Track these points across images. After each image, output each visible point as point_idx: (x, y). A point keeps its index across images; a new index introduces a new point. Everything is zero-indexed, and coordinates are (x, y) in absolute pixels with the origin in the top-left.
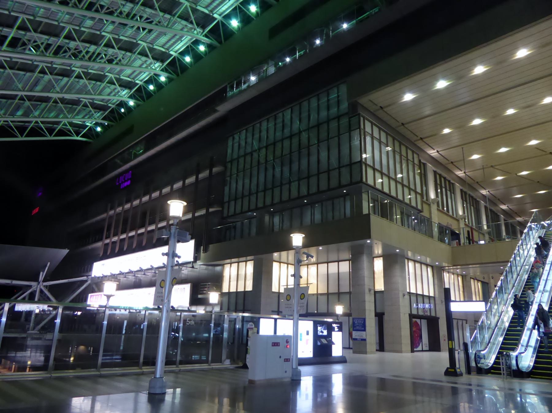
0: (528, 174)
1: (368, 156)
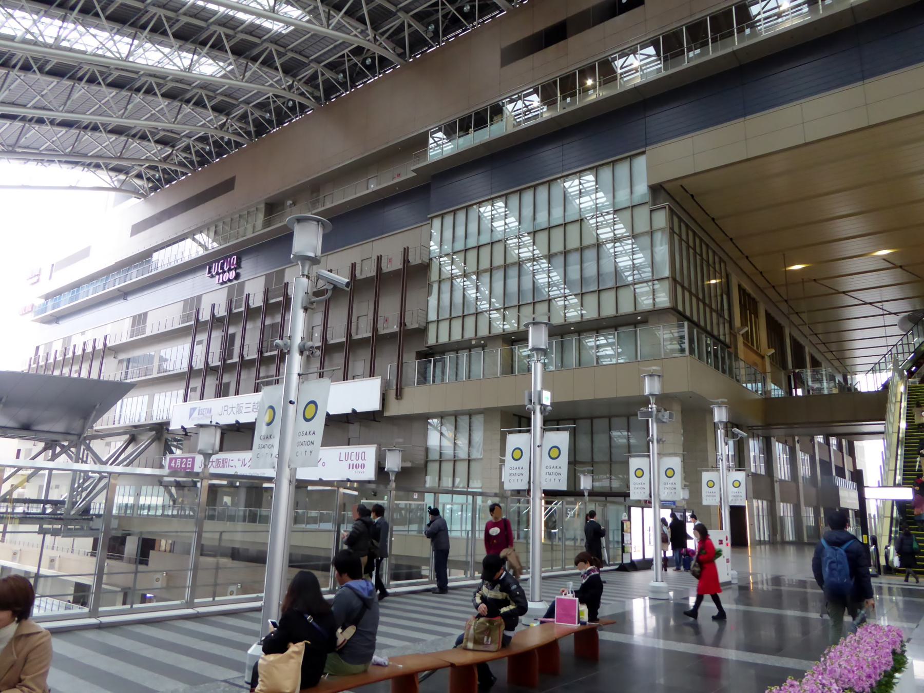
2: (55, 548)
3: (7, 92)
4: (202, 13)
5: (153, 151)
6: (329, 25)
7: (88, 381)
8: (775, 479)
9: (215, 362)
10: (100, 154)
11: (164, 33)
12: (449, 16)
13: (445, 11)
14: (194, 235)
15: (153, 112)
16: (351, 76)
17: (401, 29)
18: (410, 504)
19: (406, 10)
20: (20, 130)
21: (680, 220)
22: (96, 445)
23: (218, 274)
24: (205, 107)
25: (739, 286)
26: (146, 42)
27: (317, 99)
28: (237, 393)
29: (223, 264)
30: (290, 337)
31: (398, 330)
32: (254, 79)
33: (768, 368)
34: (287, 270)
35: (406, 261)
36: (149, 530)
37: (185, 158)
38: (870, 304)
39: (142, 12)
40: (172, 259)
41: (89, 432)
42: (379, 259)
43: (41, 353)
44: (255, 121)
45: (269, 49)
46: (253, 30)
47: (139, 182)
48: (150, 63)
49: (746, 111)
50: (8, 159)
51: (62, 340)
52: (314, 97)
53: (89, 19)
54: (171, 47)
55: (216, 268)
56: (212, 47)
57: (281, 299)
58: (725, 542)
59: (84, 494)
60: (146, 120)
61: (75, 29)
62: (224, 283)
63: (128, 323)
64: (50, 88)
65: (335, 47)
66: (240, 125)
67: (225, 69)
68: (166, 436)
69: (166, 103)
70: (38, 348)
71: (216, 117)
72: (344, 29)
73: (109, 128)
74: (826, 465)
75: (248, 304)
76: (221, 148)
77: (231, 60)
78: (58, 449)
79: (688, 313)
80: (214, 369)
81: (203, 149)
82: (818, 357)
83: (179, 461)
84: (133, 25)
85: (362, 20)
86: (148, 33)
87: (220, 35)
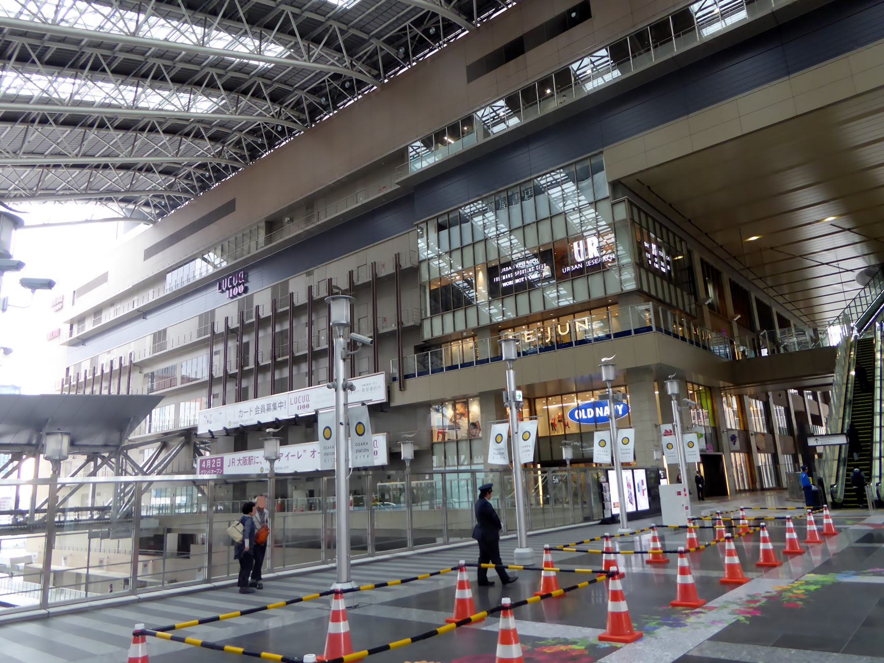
2: (102, 550)
5: (158, 181)
6: (310, 57)
7: (118, 397)
8: (750, 433)
9: (233, 370)
11: (164, 79)
12: (417, 39)
13: (413, 34)
14: (203, 255)
15: (156, 147)
16: (332, 99)
17: (375, 53)
18: (421, 484)
19: (378, 36)
21: (639, 210)
22: (133, 453)
23: (228, 289)
24: (202, 138)
25: (702, 260)
27: (303, 121)
28: (256, 397)
29: (231, 280)
30: (336, 380)
31: (396, 328)
33: (736, 332)
34: (290, 281)
35: (398, 265)
36: (188, 529)
38: (827, 264)
39: (79, 53)
40: (185, 279)
41: (126, 443)
43: (71, 373)
44: (248, 145)
45: (257, 83)
46: (242, 68)
47: (146, 210)
49: (687, 109)
51: (89, 361)
52: (299, 120)
53: (98, 74)
54: (170, 90)
55: (226, 283)
57: (288, 308)
58: (683, 493)
59: (126, 499)
60: (148, 156)
62: (234, 297)
63: (149, 341)
64: (65, 135)
66: (234, 151)
67: (218, 104)
68: (194, 440)
69: (168, 138)
70: (68, 369)
71: (213, 146)
72: (322, 58)
74: (801, 416)
75: (259, 316)
76: (219, 173)
77: (223, 96)
78: (99, 461)
79: (653, 293)
80: (233, 376)
81: (203, 175)
82: (786, 315)
83: (209, 462)
84: (135, 76)
85: (339, 50)
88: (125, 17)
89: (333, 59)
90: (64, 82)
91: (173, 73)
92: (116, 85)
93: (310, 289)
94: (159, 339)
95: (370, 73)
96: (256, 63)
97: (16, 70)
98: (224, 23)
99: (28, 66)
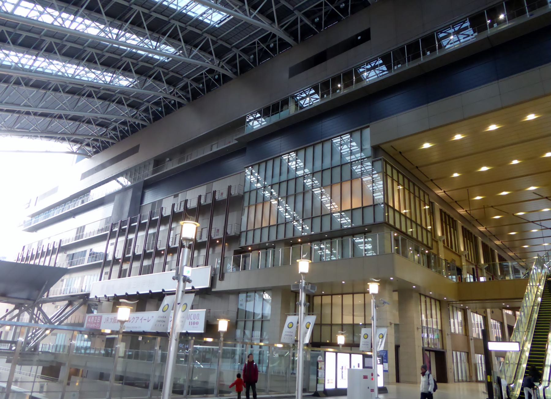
0: (509, 194)
1: (407, 211)
3: (44, 102)
4: (117, 51)
5: (95, 130)
8: (470, 338)
9: (119, 255)
10: (63, 132)
11: (130, 71)
13: (260, 48)
20: (49, 122)
26: (120, 76)
27: (188, 99)
32: (150, 88)
37: (114, 134)
39: (82, 51)
42: (215, 192)
43: (26, 251)
47: (87, 148)
48: (90, 80)
50: (11, 135)
52: (186, 98)
53: (92, 65)
56: (88, 61)
59: (35, 339)
60: (90, 112)
61: (83, 70)
65: (197, 69)
70: (24, 247)
73: (69, 117)
76: (134, 129)
84: (114, 67)
86: (85, 62)
87: (128, 63)
88: (112, 32)
89: (208, 60)
90: (71, 67)
91: (136, 68)
92: (102, 72)
93: (173, 205)
94: (80, 233)
95: (232, 71)
96: (125, 48)
97: (45, 57)
98: (134, 28)
99: (52, 55)
